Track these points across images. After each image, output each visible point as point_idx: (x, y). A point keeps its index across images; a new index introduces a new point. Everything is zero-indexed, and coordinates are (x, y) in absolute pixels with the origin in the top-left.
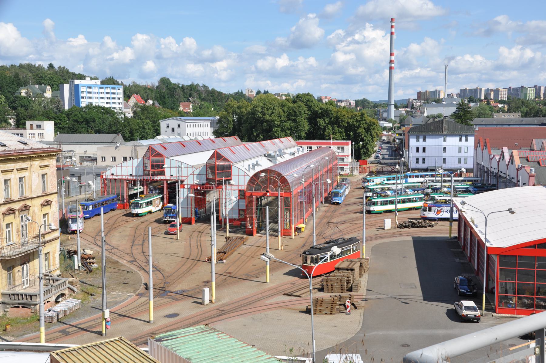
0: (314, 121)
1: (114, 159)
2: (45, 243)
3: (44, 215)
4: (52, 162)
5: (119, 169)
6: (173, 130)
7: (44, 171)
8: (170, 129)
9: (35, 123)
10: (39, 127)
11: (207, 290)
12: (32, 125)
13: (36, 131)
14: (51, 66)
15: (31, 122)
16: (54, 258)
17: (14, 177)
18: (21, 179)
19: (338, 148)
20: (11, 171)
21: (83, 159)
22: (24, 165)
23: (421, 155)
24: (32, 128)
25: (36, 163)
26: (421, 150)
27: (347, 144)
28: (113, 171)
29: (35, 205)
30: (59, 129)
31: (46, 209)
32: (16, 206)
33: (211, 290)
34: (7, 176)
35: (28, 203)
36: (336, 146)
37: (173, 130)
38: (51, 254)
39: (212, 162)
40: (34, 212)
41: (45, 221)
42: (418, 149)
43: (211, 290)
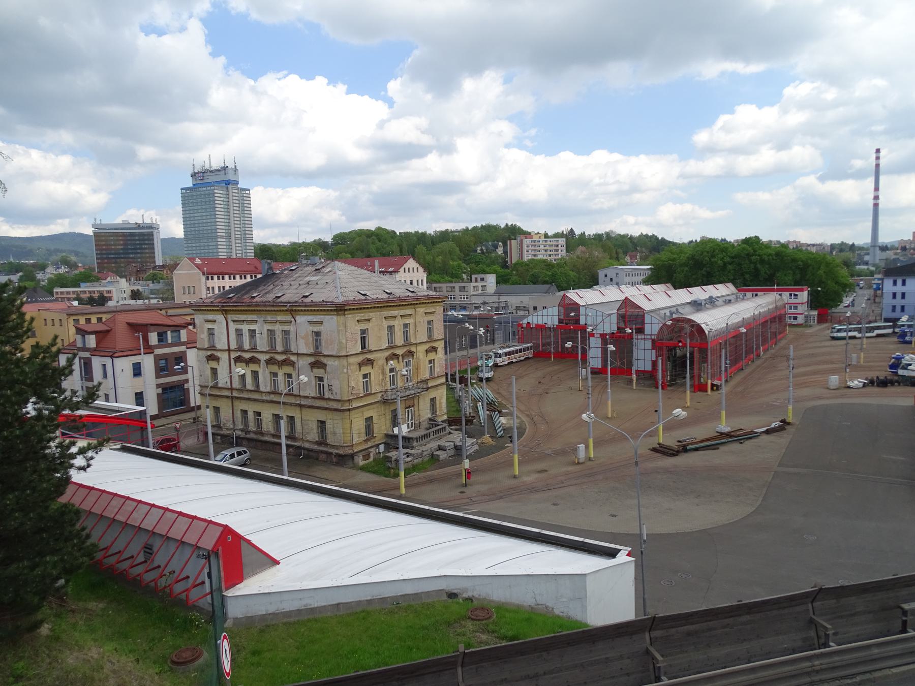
0: (747, 264)
1: (535, 308)
2: (427, 389)
3: (430, 362)
4: (439, 309)
5: (535, 318)
6: (611, 280)
7: (430, 318)
8: (608, 279)
9: (479, 276)
10: (482, 279)
11: (582, 446)
12: (476, 279)
13: (480, 284)
14: (507, 225)
15: (476, 276)
16: (440, 403)
17: (398, 324)
18: (406, 326)
19: (791, 295)
20: (395, 317)
21: (518, 308)
22: (409, 311)
23: (899, 301)
24: (476, 281)
25: (421, 310)
26: (899, 296)
27: (802, 290)
28: (529, 320)
29: (420, 351)
30: (501, 280)
31: (432, 356)
32: (400, 352)
33: (587, 447)
34: (391, 323)
35: (413, 349)
36: (788, 294)
37: (611, 280)
38: (438, 399)
39: (623, 311)
40: (418, 358)
41: (214, 371)
42: (894, 295)
43: (587, 447)
